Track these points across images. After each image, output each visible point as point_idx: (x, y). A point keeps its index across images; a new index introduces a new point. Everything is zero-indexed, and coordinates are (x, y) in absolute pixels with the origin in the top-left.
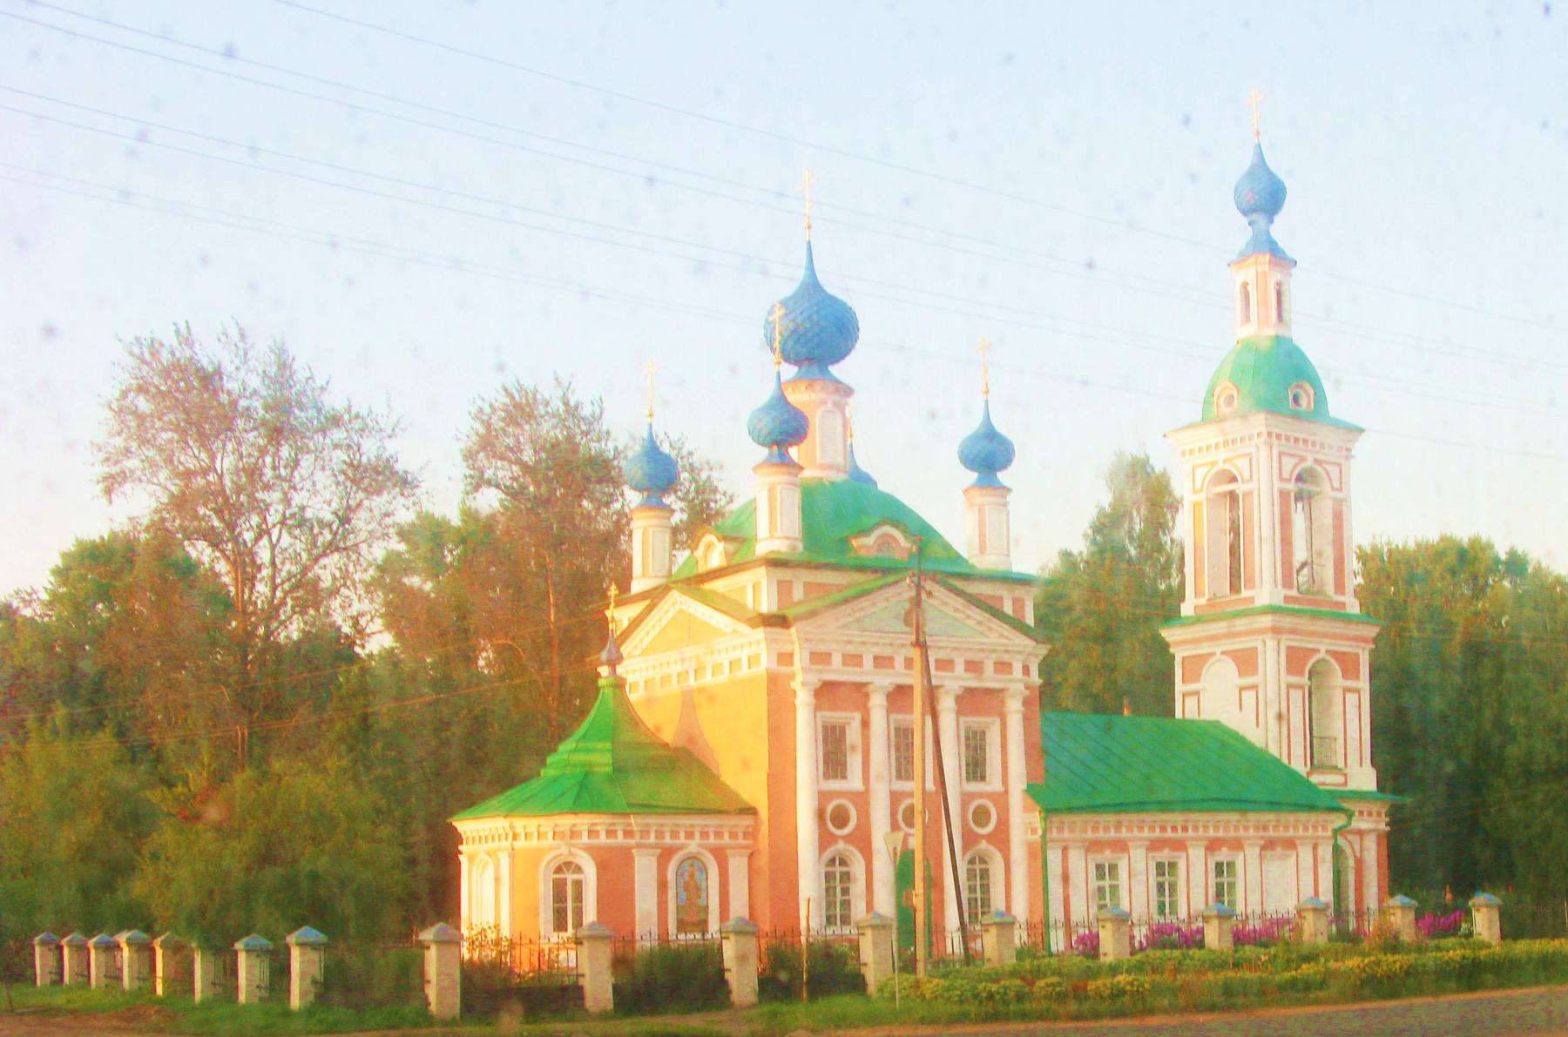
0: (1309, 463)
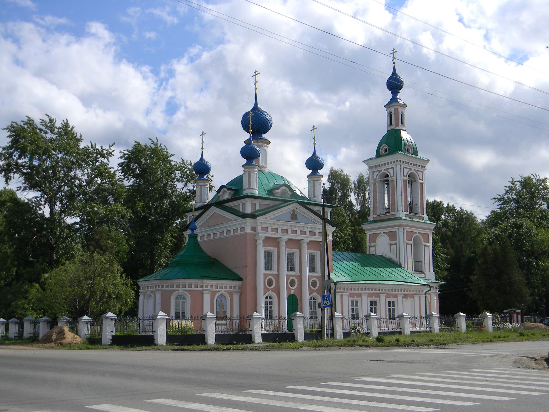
0: (413, 171)
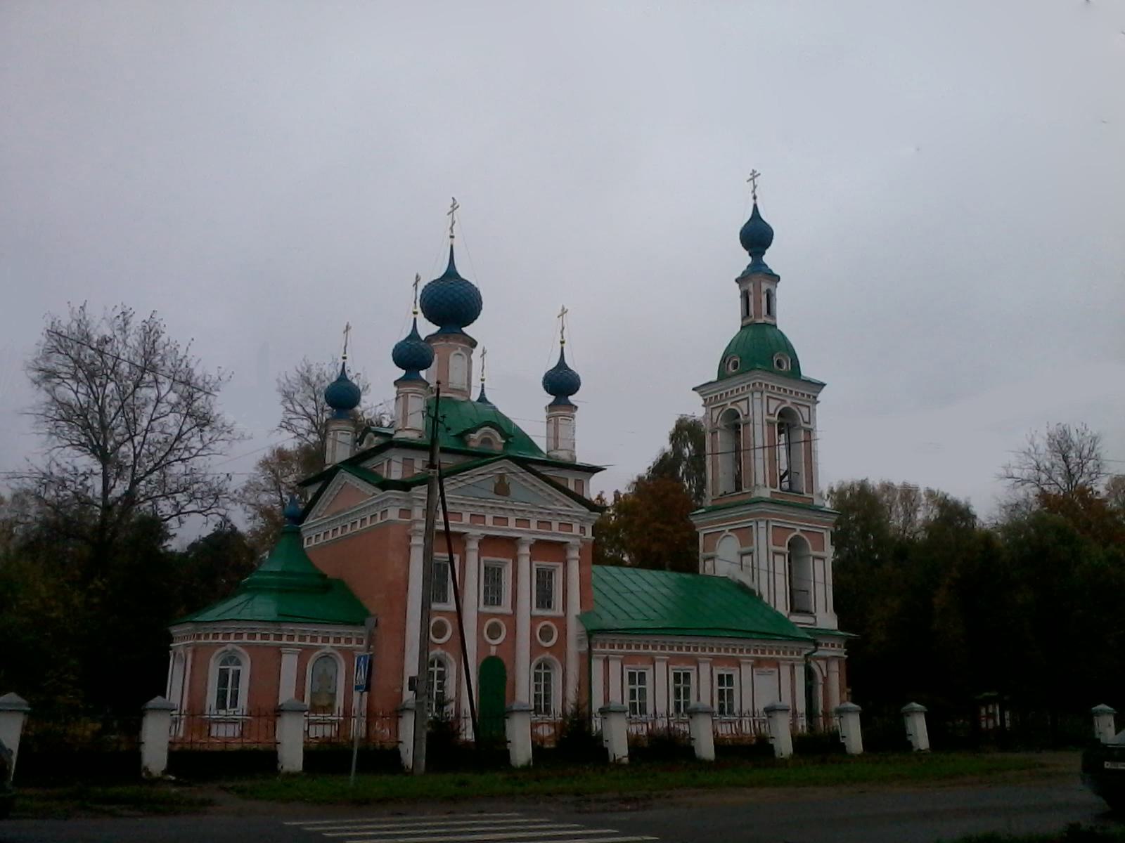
0: (788, 403)
